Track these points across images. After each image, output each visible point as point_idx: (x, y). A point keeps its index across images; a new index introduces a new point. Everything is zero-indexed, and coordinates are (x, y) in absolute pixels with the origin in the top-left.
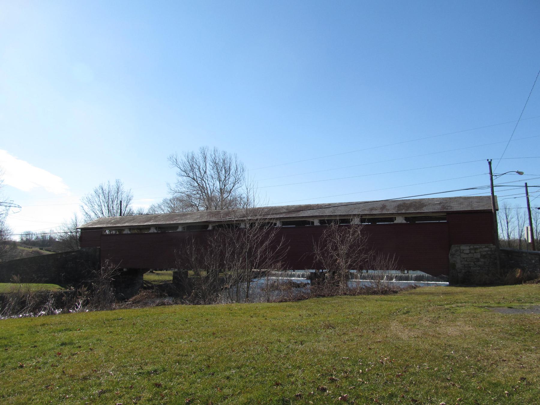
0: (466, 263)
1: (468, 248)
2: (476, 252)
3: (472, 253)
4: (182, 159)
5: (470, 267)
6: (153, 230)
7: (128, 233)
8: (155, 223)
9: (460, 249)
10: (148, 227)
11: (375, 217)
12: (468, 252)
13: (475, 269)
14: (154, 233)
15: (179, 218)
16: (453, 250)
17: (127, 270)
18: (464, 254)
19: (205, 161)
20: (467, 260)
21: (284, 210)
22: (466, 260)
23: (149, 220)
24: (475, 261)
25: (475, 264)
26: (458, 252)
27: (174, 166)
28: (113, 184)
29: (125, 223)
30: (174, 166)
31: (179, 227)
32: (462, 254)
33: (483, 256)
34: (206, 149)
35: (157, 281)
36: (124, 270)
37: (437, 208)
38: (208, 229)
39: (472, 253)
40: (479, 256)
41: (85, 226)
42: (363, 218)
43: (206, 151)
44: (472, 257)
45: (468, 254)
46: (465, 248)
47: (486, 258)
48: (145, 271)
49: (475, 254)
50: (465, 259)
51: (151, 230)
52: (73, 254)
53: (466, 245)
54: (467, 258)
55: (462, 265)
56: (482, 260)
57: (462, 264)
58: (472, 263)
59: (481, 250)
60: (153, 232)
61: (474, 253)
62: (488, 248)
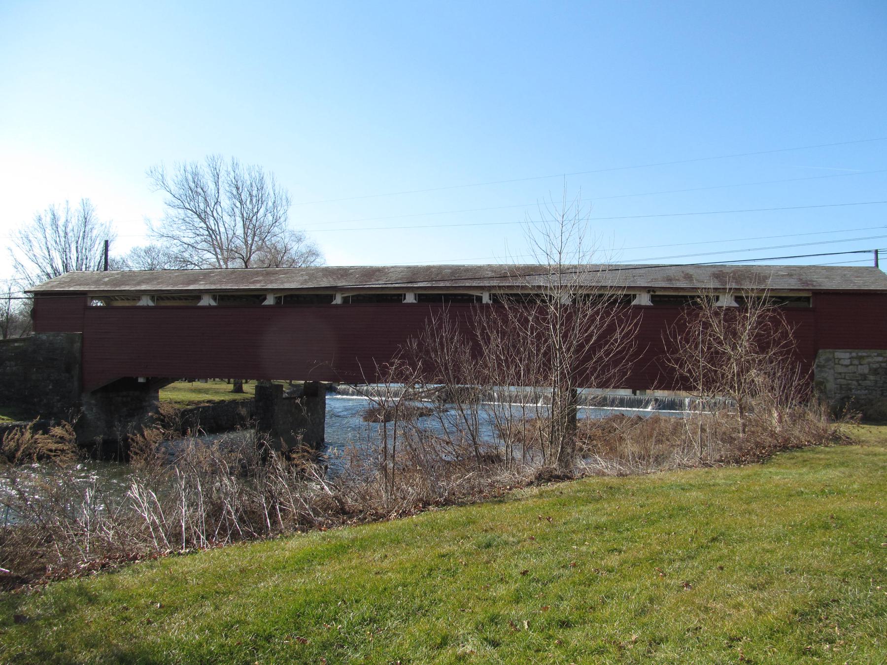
0: (843, 382)
1: (847, 355)
2: (862, 363)
3: (854, 365)
4: (173, 177)
5: (850, 390)
6: (146, 302)
7: (148, 306)
8: (213, 287)
9: (834, 357)
10: (198, 295)
11: (680, 294)
12: (847, 362)
13: (859, 392)
14: (147, 308)
15: (261, 278)
16: (821, 359)
17: (145, 381)
18: (840, 366)
19: (217, 183)
20: (845, 376)
21: (490, 274)
22: (843, 377)
23: (195, 281)
24: (860, 378)
25: (859, 385)
26: (830, 362)
27: (159, 187)
28: (76, 207)
29: (139, 284)
30: (159, 187)
31: (268, 297)
32: (836, 366)
33: (875, 372)
34: (218, 159)
35: (179, 402)
36: (139, 381)
37: (793, 284)
38: (332, 303)
39: (854, 365)
40: (866, 371)
41: (44, 288)
42: (656, 294)
43: (219, 163)
44: (855, 373)
45: (847, 366)
46: (843, 355)
47: (878, 374)
48: (163, 382)
49: (859, 367)
50: (843, 375)
51: (202, 301)
52: (16, 344)
53: (844, 350)
54: (845, 373)
55: (836, 386)
56: (872, 378)
57: (837, 384)
58: (855, 382)
59: (870, 360)
60: (208, 305)
61: (857, 365)
62: (882, 356)
